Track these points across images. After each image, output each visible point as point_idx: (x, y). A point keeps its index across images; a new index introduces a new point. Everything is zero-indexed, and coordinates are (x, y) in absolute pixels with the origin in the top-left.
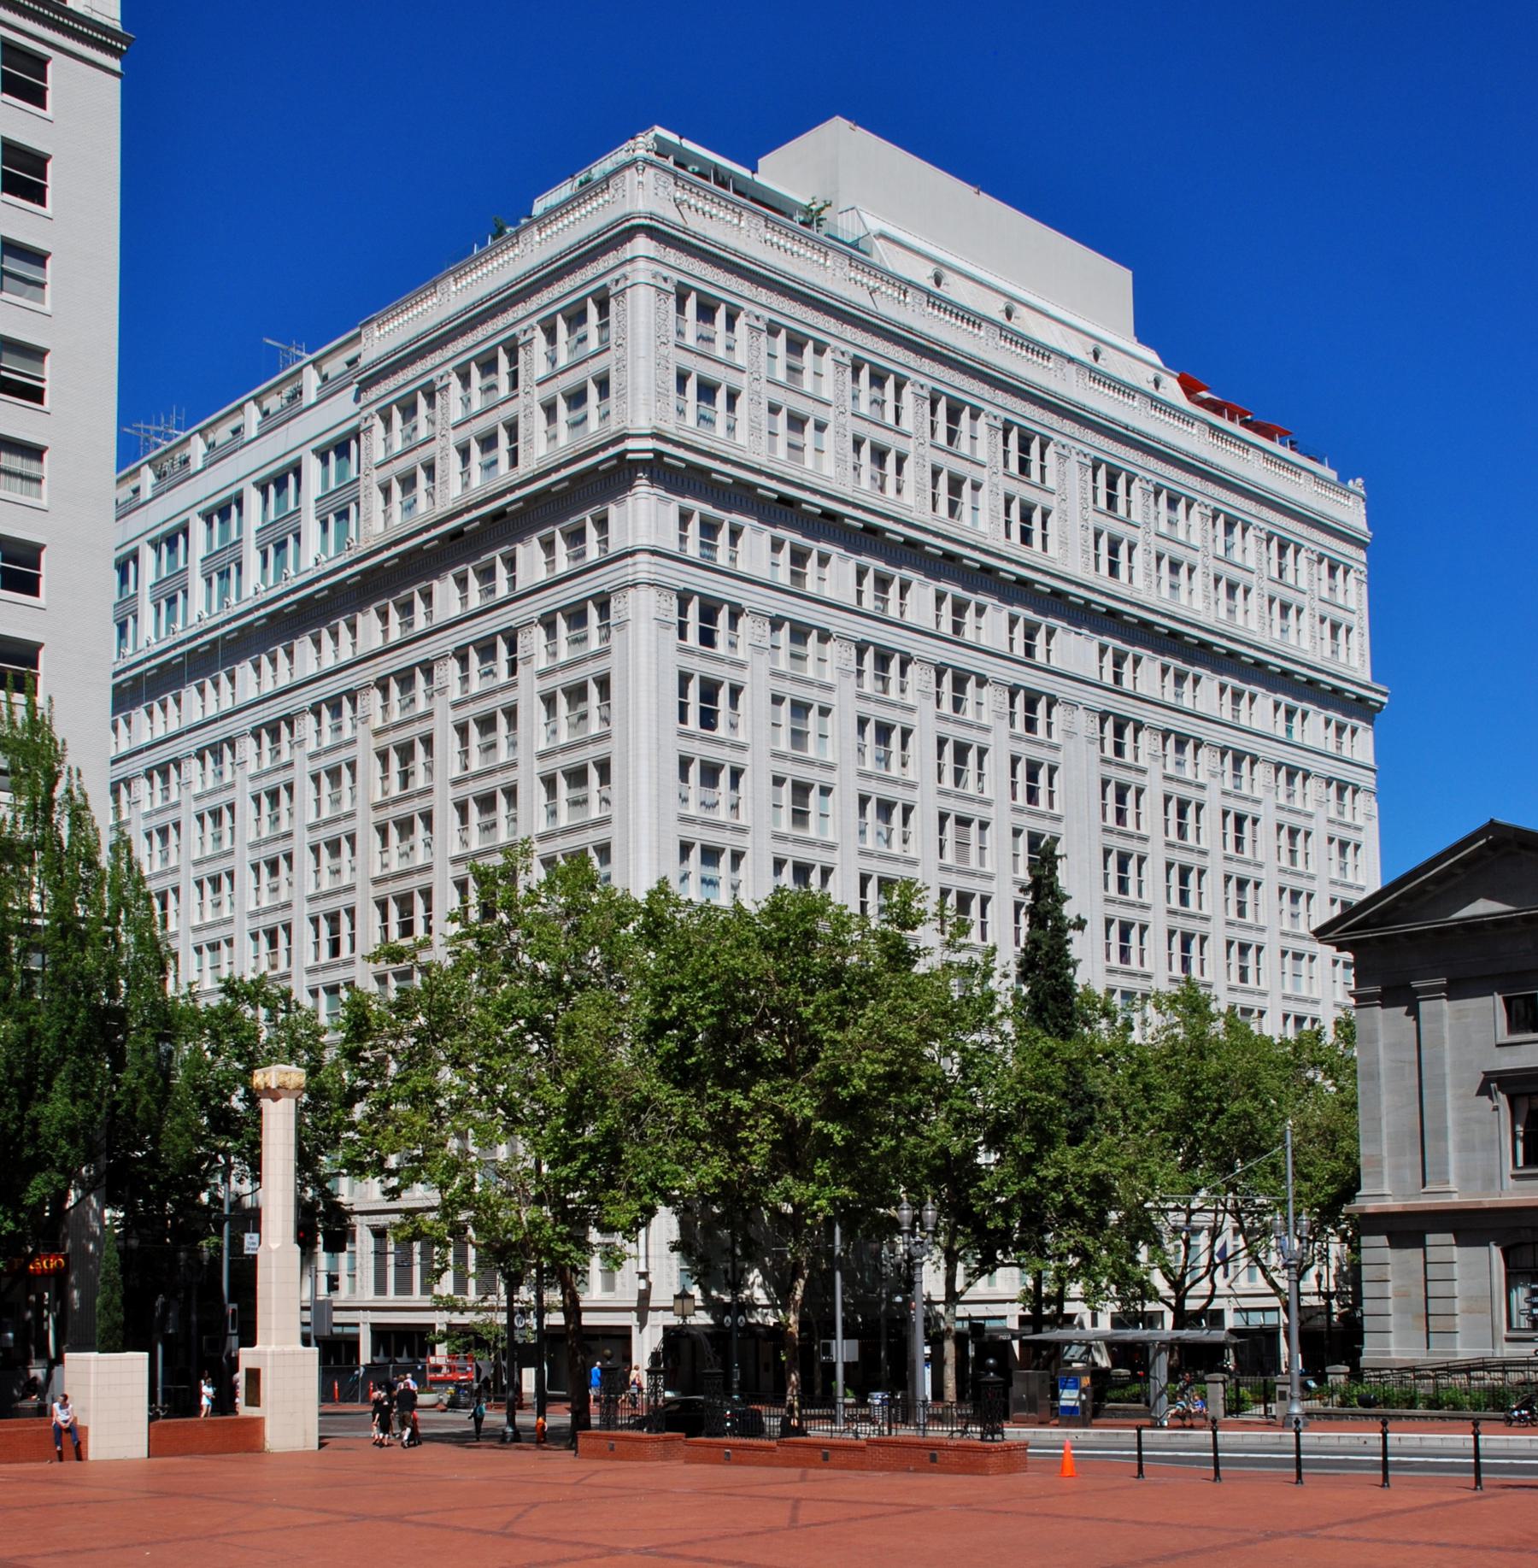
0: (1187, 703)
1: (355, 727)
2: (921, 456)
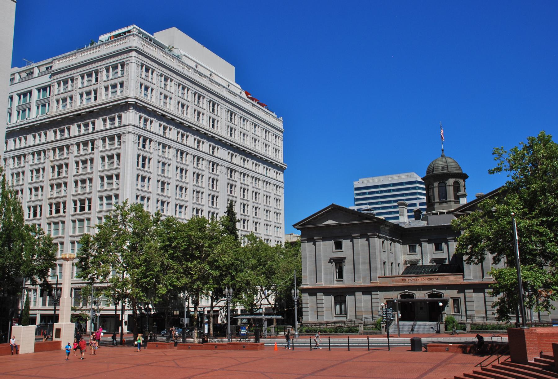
0: (245, 166)
1: (45, 159)
2: (192, 107)
